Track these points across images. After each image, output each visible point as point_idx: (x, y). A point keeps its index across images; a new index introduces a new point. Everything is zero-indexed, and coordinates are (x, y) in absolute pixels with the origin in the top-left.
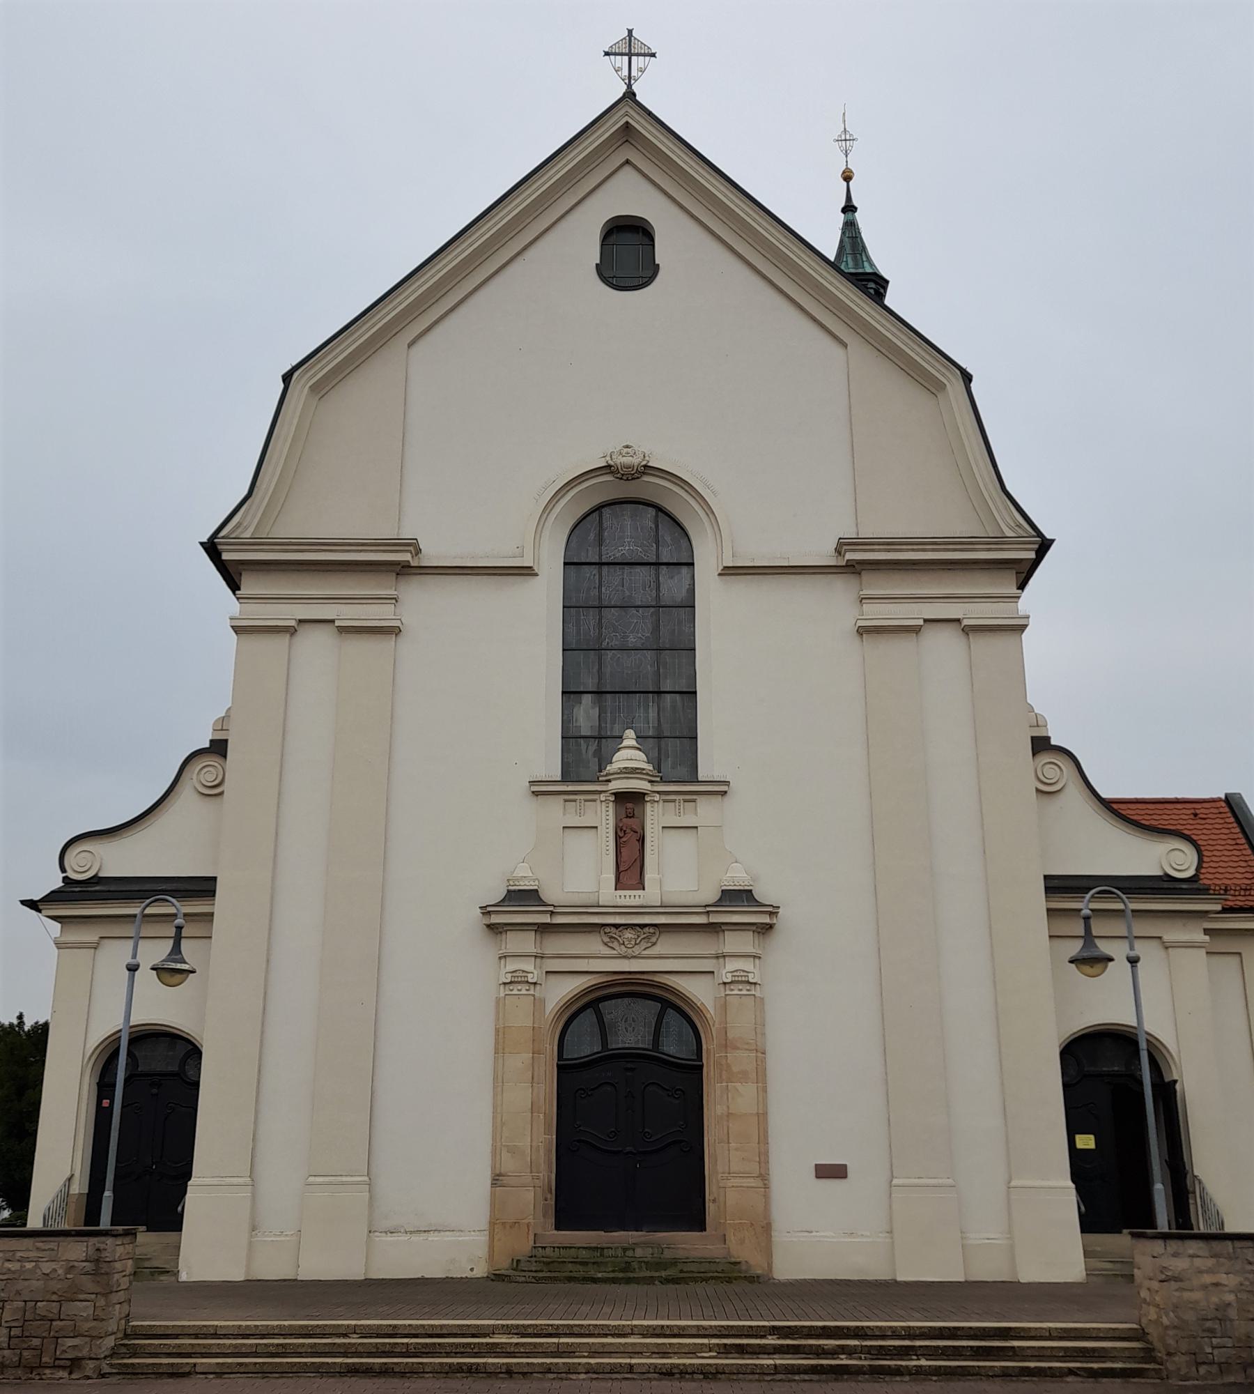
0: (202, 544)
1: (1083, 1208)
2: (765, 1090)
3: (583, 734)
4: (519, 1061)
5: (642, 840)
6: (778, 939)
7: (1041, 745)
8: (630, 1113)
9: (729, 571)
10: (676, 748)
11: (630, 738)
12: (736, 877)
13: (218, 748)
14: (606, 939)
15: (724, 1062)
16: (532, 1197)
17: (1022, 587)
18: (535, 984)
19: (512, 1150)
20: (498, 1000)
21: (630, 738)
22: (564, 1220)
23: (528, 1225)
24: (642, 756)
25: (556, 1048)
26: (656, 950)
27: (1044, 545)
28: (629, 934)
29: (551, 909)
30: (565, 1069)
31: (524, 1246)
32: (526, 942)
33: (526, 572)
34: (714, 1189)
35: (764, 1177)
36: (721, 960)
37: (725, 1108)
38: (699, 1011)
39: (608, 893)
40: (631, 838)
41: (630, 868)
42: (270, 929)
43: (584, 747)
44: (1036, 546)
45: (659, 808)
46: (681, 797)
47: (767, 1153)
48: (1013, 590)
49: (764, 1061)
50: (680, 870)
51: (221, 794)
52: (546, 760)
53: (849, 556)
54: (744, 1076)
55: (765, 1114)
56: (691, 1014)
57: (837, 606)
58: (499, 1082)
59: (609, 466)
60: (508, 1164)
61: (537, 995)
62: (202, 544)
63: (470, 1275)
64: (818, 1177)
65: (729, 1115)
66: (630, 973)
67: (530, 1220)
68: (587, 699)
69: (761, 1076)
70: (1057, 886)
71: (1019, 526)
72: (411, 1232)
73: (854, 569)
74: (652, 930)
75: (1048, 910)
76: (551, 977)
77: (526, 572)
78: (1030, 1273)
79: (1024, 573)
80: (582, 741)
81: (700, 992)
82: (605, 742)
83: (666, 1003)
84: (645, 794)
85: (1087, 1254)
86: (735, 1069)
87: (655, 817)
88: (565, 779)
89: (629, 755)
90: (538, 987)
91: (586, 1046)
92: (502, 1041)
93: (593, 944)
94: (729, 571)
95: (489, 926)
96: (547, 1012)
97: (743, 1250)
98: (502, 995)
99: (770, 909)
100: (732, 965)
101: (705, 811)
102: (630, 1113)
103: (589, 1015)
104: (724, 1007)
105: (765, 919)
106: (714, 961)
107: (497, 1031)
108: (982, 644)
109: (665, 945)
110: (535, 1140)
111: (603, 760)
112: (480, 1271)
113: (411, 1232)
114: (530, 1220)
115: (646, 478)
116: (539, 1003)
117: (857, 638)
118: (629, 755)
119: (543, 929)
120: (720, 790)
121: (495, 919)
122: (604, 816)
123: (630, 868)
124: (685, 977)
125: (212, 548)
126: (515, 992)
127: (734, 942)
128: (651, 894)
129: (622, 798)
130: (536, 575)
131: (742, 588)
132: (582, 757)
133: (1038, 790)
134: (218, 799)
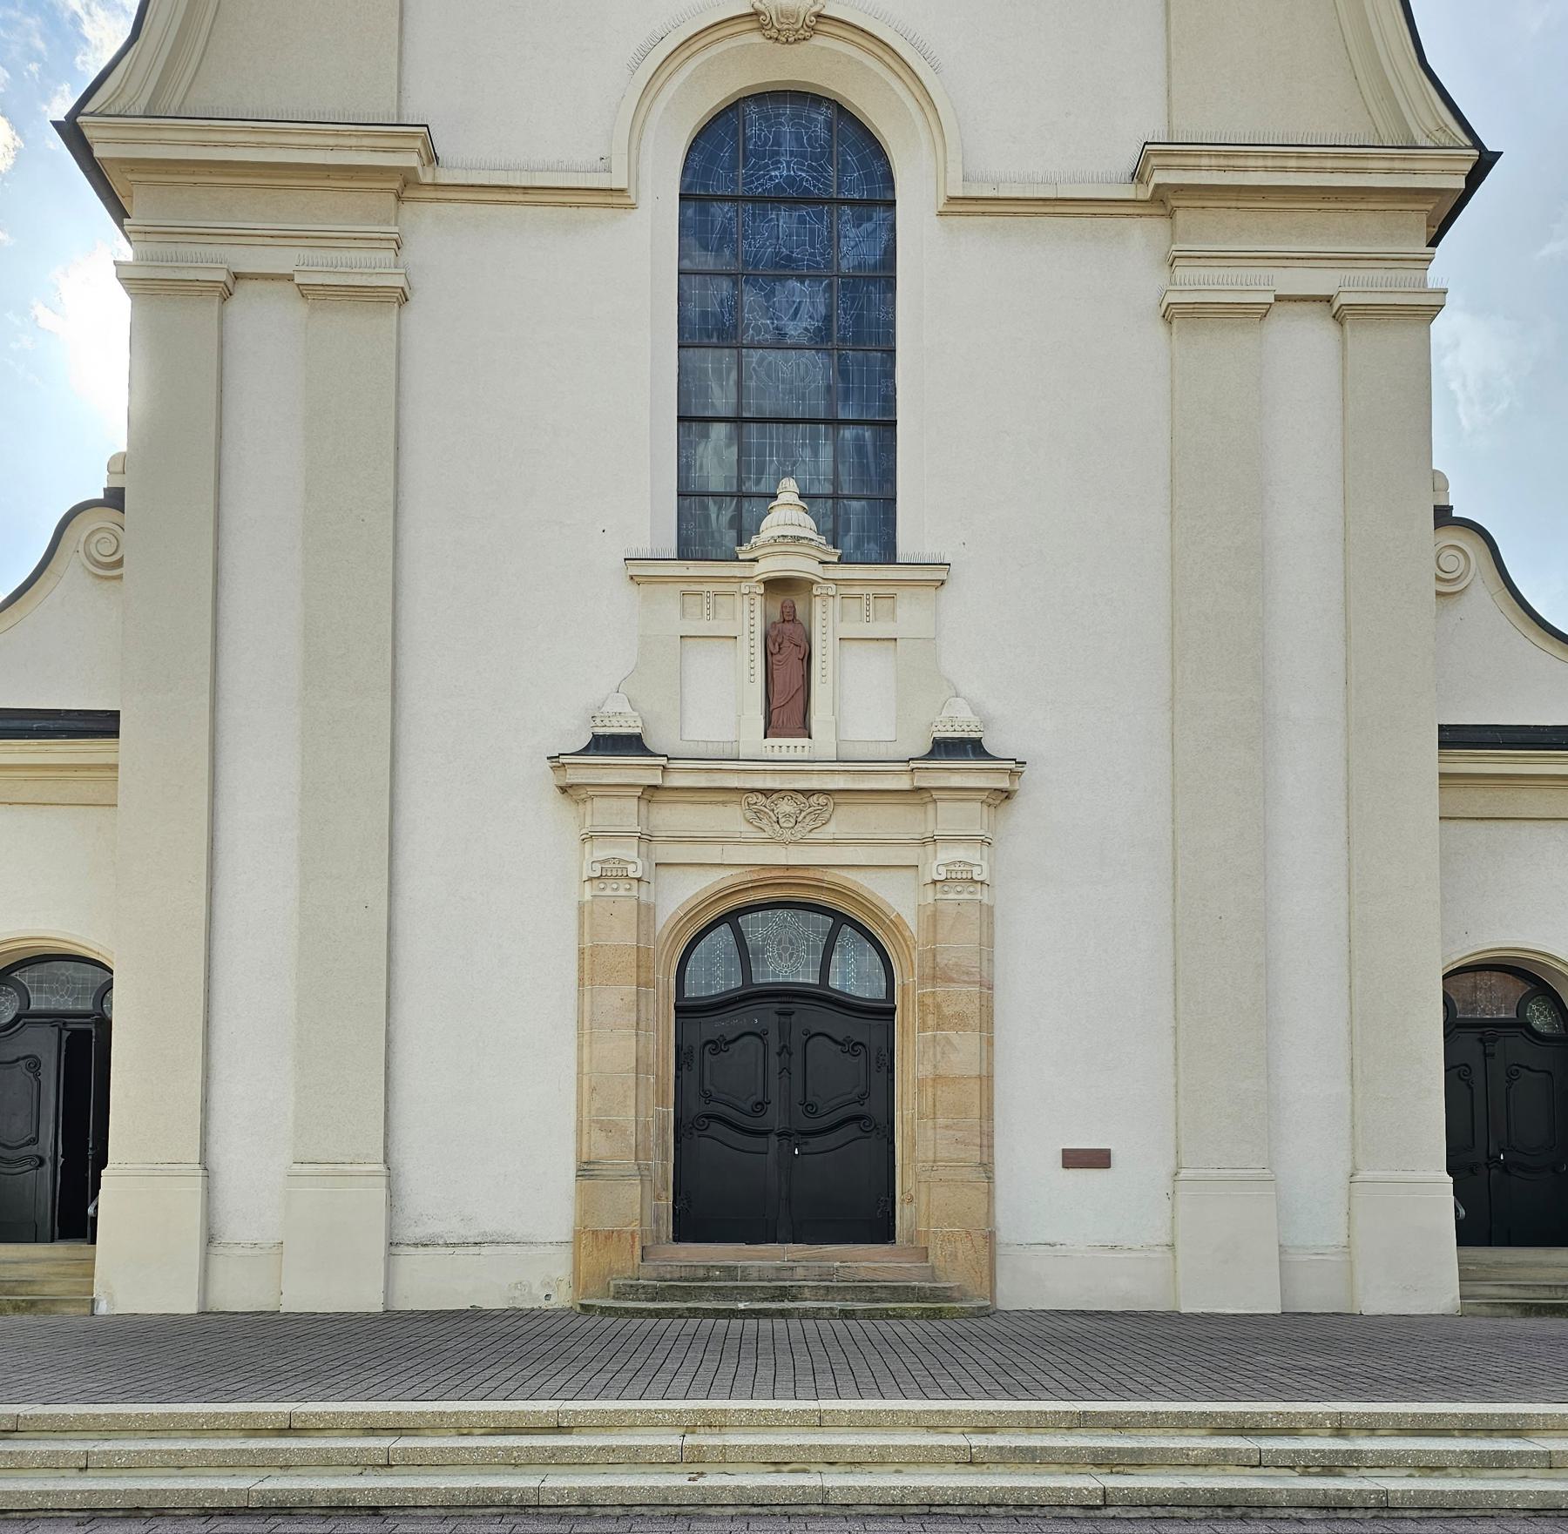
0: (56, 124)
1: (1462, 1212)
2: (990, 1043)
3: (712, 488)
4: (618, 996)
5: (807, 659)
6: (1020, 812)
7: (1443, 516)
8: (781, 1109)
9: (960, 205)
10: (863, 517)
11: (788, 490)
12: (959, 723)
13: (115, 498)
14: (749, 815)
15: (929, 1001)
16: (642, 1200)
17: (1434, 242)
18: (639, 880)
19: (606, 1128)
20: (581, 907)
21: (788, 490)
22: (691, 1223)
23: (632, 1234)
24: (811, 523)
25: (673, 981)
26: (831, 831)
27: (1485, 162)
28: (786, 807)
29: (663, 761)
30: (686, 1011)
31: (625, 1264)
32: (626, 813)
33: (614, 198)
34: (910, 1184)
35: (987, 1168)
36: (930, 848)
37: (930, 1067)
38: (896, 926)
39: (749, 734)
40: (791, 655)
41: (787, 708)
42: (221, 346)
43: (713, 509)
44: (1469, 166)
45: (834, 605)
46: (871, 590)
47: (991, 1135)
48: (1423, 248)
49: (990, 999)
50: (864, 705)
51: (120, 577)
52: (653, 521)
53: (1160, 177)
54: (961, 1021)
55: (990, 1077)
56: (879, 933)
57: (1133, 260)
58: (588, 1027)
59: (756, 14)
60: (601, 1146)
61: (643, 898)
62: (56, 124)
63: (544, 1305)
64: (1066, 1165)
65: (937, 1079)
66: (788, 867)
67: (635, 1226)
68: (719, 431)
69: (986, 1021)
70: (1454, 738)
71: (1443, 129)
72: (454, 1245)
73: (1164, 201)
74: (822, 800)
75: (1442, 775)
76: (663, 871)
77: (614, 198)
78: (1378, 1299)
79: (1444, 213)
80: (710, 501)
81: (897, 899)
82: (747, 503)
83: (842, 921)
84: (812, 583)
85: (1464, 1277)
86: (948, 1011)
87: (828, 624)
88: (684, 554)
89: (787, 516)
90: (644, 885)
91: (715, 976)
92: (592, 966)
93: (731, 818)
94: (960, 205)
95: (564, 790)
96: (659, 927)
97: (953, 1267)
98: (588, 897)
99: (1012, 765)
100: (947, 854)
101: (910, 615)
102: (781, 1109)
103: (724, 933)
104: (933, 919)
105: (1004, 783)
106: (919, 850)
107: (581, 952)
108: (1367, 341)
109: (843, 822)
110: (644, 1111)
111: (743, 530)
112: (562, 1299)
113: (454, 1245)
114: (635, 1226)
115: (818, 41)
116: (645, 912)
117: (1160, 329)
118: (787, 516)
119: (651, 792)
120: (936, 575)
121: (573, 777)
122: (747, 619)
123: (787, 708)
124: (872, 874)
125: (71, 131)
126: (608, 892)
127: (951, 817)
128: (824, 738)
129: (777, 586)
130: (633, 207)
131: (975, 233)
132: (709, 523)
133: (1439, 594)
134: (114, 583)
